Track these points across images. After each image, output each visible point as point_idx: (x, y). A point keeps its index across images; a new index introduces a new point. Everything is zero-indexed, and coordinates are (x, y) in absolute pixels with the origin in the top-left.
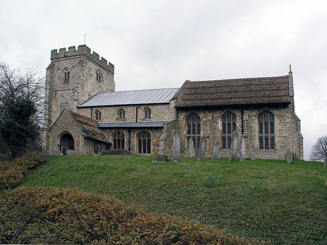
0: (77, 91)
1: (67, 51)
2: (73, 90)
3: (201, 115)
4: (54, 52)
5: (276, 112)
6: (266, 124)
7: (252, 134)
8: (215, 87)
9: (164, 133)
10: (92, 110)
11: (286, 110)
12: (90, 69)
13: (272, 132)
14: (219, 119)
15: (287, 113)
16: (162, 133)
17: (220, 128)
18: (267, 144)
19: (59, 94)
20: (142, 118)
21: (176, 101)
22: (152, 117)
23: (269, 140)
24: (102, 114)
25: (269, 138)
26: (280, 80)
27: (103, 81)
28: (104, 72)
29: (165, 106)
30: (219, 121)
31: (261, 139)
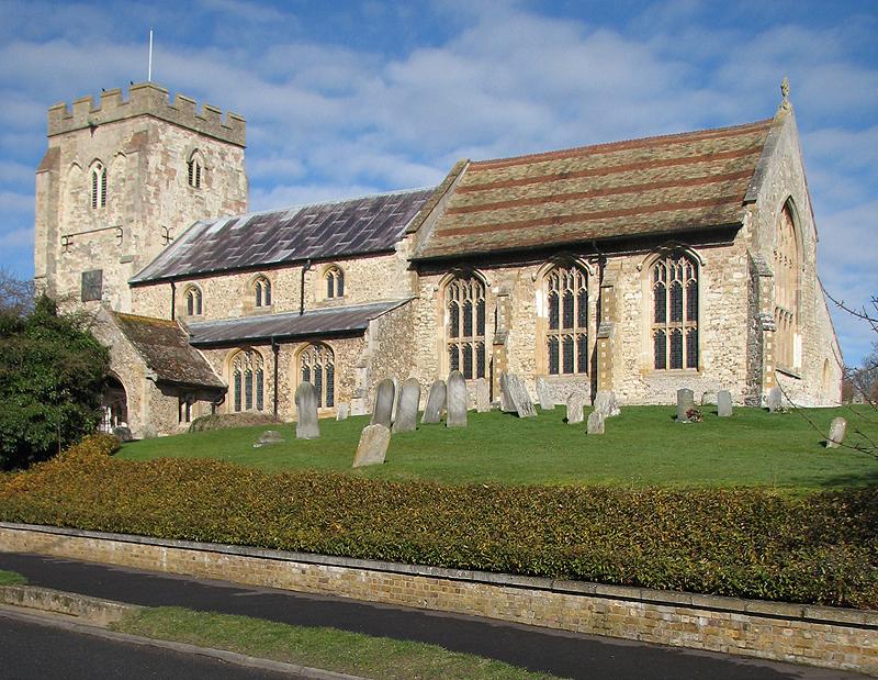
0: (129, 233)
2: (119, 227)
3: (488, 276)
10: (174, 288)
13: (694, 314)
16: (364, 345)
17: (543, 309)
18: (468, 368)
19: (77, 245)
20: (319, 300)
21: (415, 241)
22: (345, 293)
28: (211, 152)
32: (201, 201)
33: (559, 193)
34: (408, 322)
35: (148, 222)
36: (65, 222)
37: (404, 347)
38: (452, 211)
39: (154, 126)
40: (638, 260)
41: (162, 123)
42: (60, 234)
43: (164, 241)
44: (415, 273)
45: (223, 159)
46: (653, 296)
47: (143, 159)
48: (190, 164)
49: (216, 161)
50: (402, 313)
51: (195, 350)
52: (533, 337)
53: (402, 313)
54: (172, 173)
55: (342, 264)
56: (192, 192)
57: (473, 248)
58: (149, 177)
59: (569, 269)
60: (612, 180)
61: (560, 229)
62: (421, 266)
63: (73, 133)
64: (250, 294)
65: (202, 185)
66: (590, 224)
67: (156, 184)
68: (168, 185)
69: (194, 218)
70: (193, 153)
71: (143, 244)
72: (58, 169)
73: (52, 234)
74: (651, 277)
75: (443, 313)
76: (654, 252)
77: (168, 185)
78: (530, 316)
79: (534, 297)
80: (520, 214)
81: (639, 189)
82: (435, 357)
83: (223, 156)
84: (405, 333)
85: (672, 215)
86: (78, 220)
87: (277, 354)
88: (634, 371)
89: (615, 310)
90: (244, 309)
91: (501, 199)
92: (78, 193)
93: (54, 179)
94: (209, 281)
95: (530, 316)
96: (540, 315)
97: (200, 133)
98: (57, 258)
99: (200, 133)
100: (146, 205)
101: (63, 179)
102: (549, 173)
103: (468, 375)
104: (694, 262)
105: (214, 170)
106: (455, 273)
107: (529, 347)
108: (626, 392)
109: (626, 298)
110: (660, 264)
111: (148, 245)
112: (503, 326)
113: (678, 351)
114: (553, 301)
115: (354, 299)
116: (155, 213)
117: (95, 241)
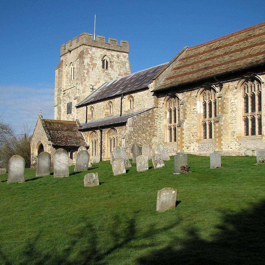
3: (180, 96)
20: (127, 110)
21: (156, 83)
28: (113, 56)
32: (108, 74)
33: (212, 56)
34: (152, 119)
35: (84, 84)
36: (64, 85)
37: (149, 128)
38: (175, 69)
39: (87, 49)
40: (235, 83)
41: (90, 47)
42: (63, 90)
43: (91, 90)
44: (155, 96)
45: (118, 58)
46: (243, 100)
47: (81, 61)
48: (103, 61)
49: (115, 59)
50: (149, 114)
51: (79, 132)
52: (196, 122)
53: (149, 114)
54: (95, 65)
55: (133, 95)
56: (104, 71)
57: (174, 84)
58: (84, 67)
59: (210, 90)
60: (203, 57)
61: (206, 72)
62: (158, 93)
63: (66, 54)
64: (107, 109)
65: (109, 68)
66: (217, 69)
67: (88, 70)
68: (93, 69)
69: (105, 80)
70: (104, 56)
71: (81, 92)
72: (62, 68)
73: (60, 90)
74: (242, 91)
75: (166, 113)
76: (242, 79)
77: (93, 69)
78: (195, 113)
79: (196, 104)
80: (195, 68)
81: (242, 50)
82: (163, 133)
83: (118, 57)
84: (149, 123)
85: (249, 60)
86: (67, 85)
87: (101, 133)
88: (235, 137)
89: (224, 108)
90: (105, 115)
91: (192, 62)
92: (67, 75)
93: (60, 71)
94: (96, 104)
95: (195, 113)
96: (199, 112)
97: (107, 49)
98: (62, 99)
99: (107, 49)
100: (83, 77)
101: (64, 71)
102: (212, 48)
103: (253, 133)
104: (259, 82)
105: (114, 62)
106: (170, 95)
107: (195, 127)
108: (231, 147)
109: (231, 102)
110: (246, 84)
111: (84, 92)
112: (182, 118)
113: (174, 133)
114: (205, 105)
115: (136, 109)
116: (87, 80)
117: (70, 92)
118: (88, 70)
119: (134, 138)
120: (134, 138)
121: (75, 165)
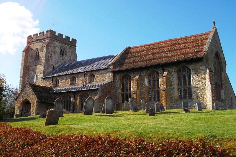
1: (38, 35)
4: (30, 37)
5: (191, 67)
6: (185, 77)
7: (172, 87)
8: (148, 50)
9: (99, 93)
10: (53, 79)
11: (201, 63)
12: (55, 47)
14: (145, 77)
15: (201, 66)
18: (185, 94)
23: (187, 91)
24: (60, 82)
25: (187, 89)
26: (151, 46)
27: (66, 54)
28: (67, 47)
29: (105, 71)
30: (146, 79)
31: (180, 90)
37: (109, 94)
52: (144, 91)
54: (55, 52)
60: (167, 49)
65: (65, 55)
67: (51, 54)
75: (120, 85)
82: (118, 97)
84: (109, 91)
85: (183, 56)
118: (51, 54)
119: (102, 100)
120: (102, 100)
121: (96, 112)
